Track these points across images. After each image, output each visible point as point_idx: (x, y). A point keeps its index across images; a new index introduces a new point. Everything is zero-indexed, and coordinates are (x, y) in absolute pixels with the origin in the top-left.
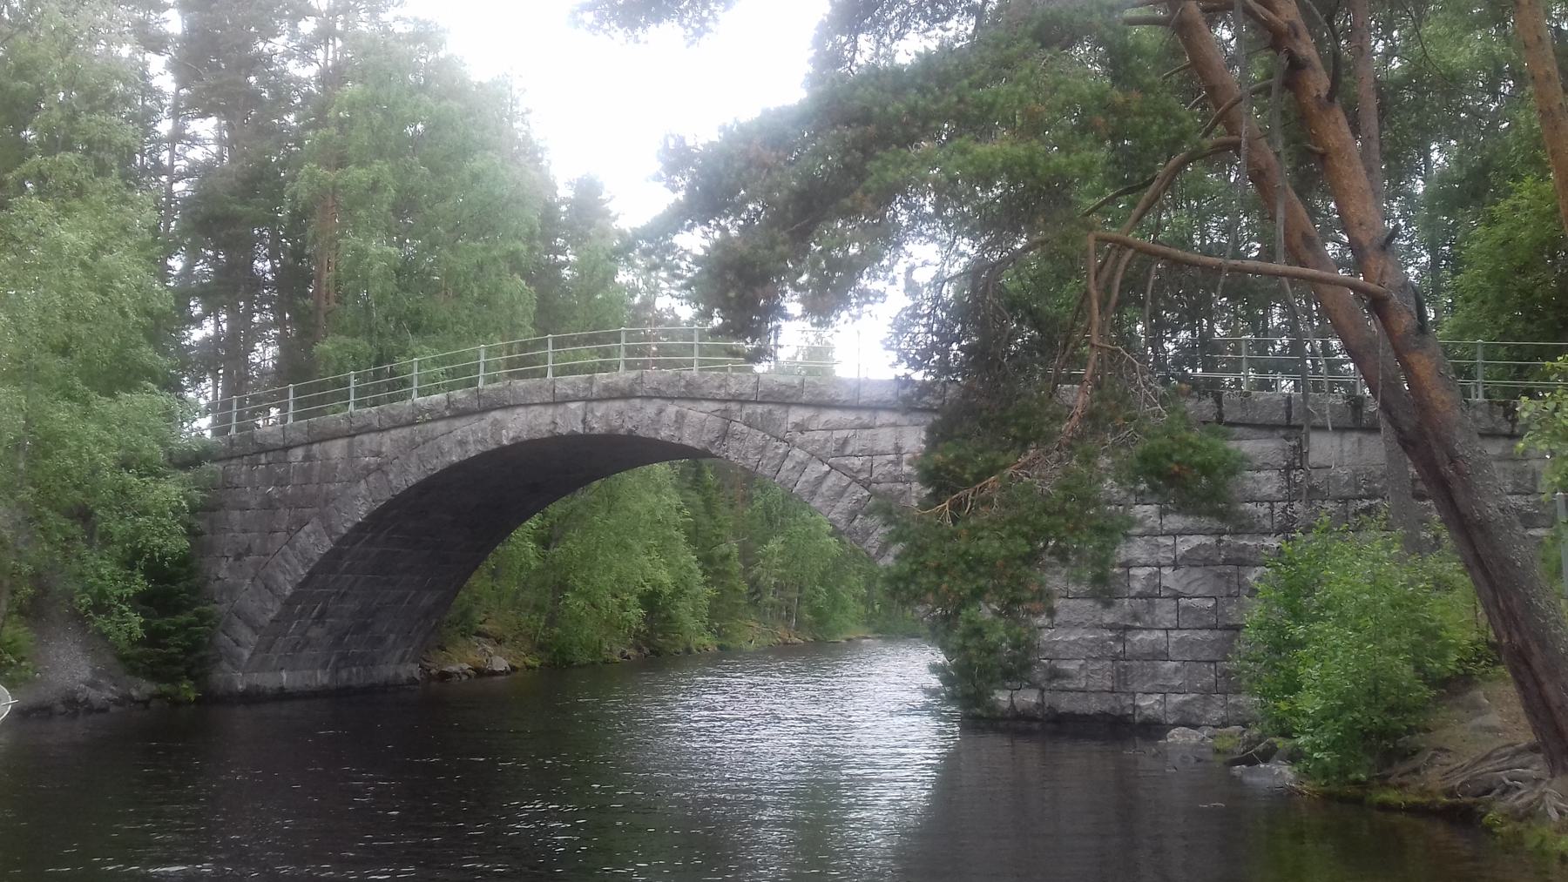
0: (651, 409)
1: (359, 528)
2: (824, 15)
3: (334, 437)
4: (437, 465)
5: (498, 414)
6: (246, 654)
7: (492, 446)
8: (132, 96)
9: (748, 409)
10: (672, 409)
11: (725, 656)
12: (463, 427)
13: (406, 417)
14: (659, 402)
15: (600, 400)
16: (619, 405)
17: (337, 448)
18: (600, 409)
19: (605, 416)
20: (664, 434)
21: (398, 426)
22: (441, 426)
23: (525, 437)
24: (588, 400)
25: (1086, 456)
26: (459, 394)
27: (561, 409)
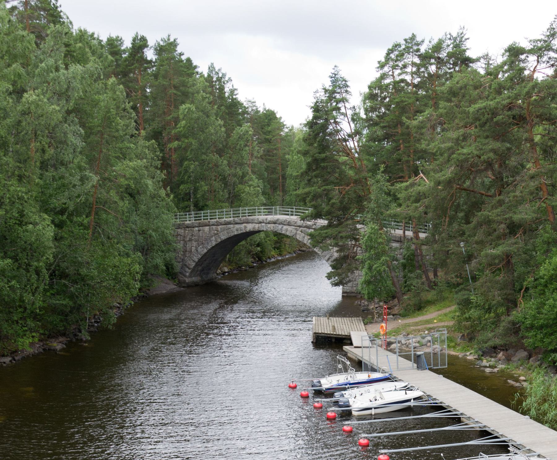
0: (280, 226)
1: (213, 247)
2: (281, 118)
3: (206, 226)
4: (232, 234)
5: (245, 224)
6: (188, 274)
7: (244, 231)
8: (409, 161)
9: (301, 228)
10: (285, 227)
11: (277, 265)
12: (237, 226)
13: (223, 223)
14: (282, 225)
15: (269, 223)
16: (273, 225)
17: (207, 229)
18: (269, 225)
19: (287, 230)
20: (283, 232)
21: (221, 224)
22: (232, 226)
23: (252, 230)
24: (266, 223)
25: (25, 161)
26: (236, 219)
27: (260, 225)
